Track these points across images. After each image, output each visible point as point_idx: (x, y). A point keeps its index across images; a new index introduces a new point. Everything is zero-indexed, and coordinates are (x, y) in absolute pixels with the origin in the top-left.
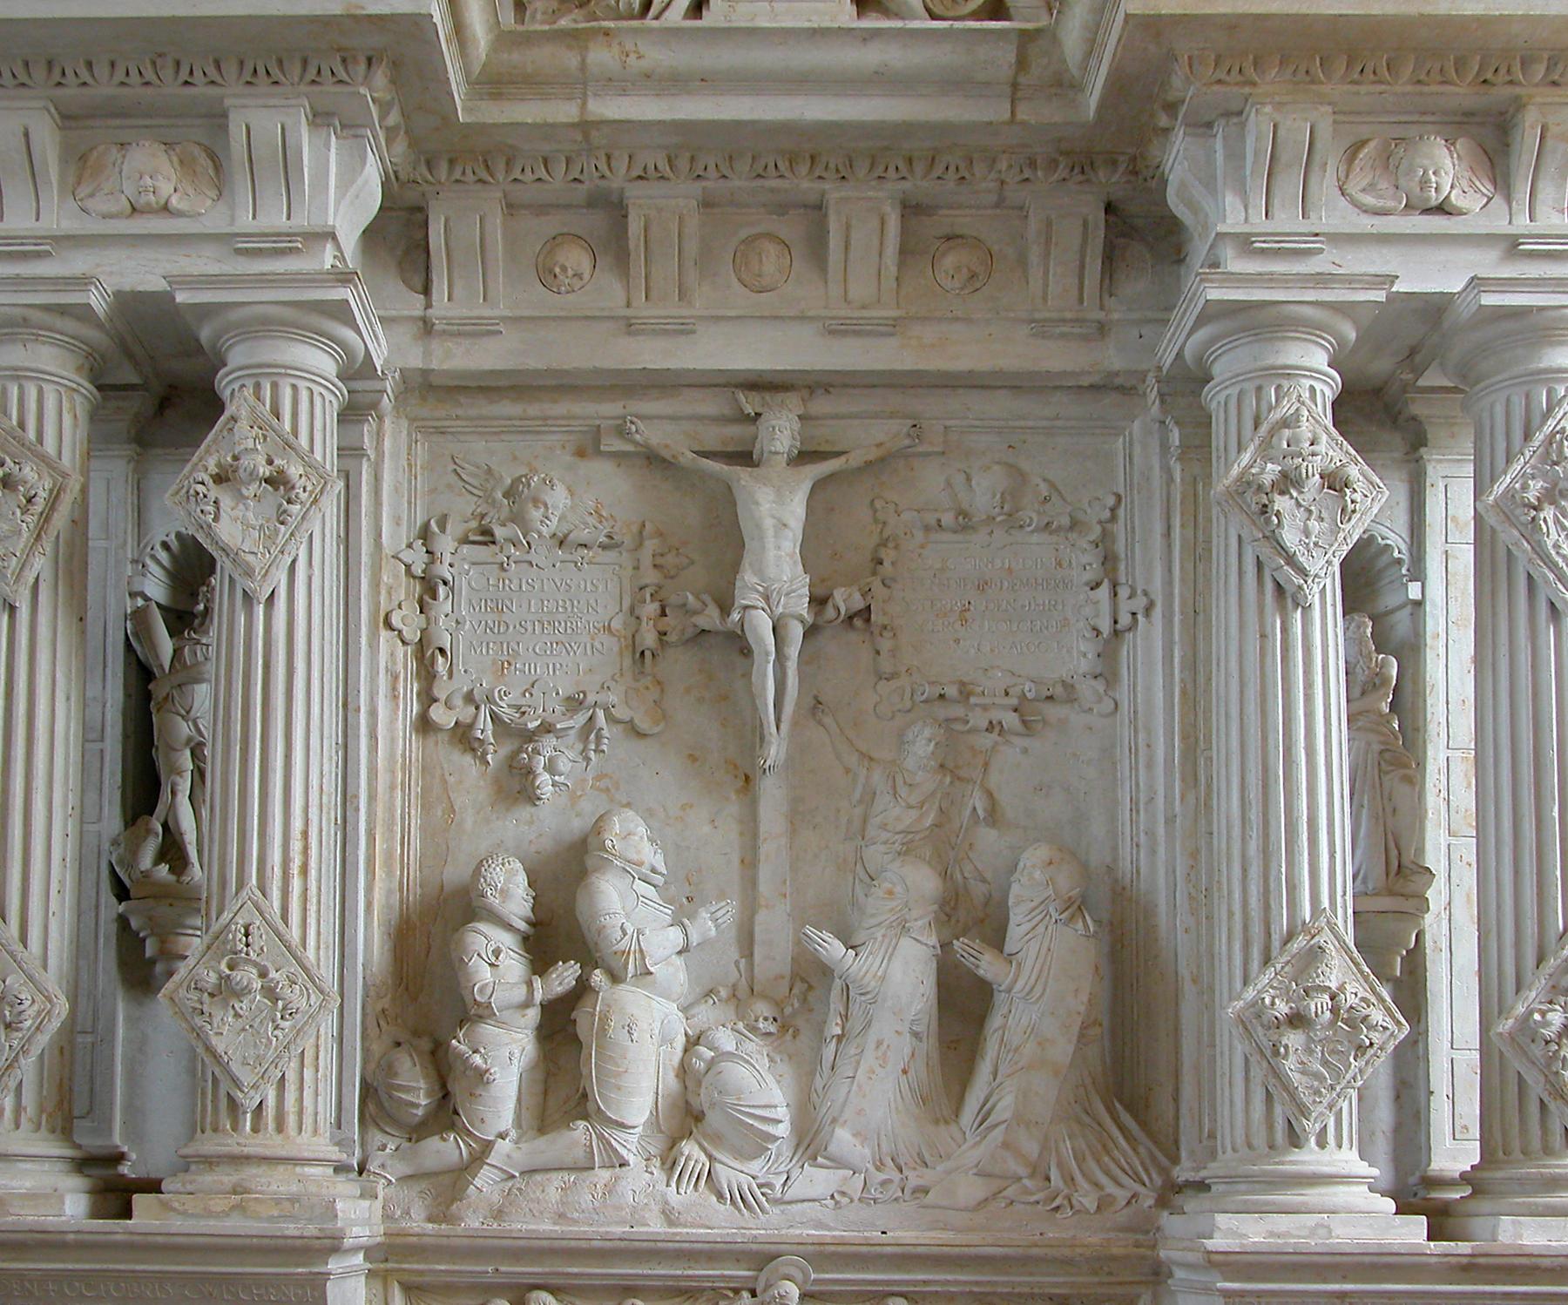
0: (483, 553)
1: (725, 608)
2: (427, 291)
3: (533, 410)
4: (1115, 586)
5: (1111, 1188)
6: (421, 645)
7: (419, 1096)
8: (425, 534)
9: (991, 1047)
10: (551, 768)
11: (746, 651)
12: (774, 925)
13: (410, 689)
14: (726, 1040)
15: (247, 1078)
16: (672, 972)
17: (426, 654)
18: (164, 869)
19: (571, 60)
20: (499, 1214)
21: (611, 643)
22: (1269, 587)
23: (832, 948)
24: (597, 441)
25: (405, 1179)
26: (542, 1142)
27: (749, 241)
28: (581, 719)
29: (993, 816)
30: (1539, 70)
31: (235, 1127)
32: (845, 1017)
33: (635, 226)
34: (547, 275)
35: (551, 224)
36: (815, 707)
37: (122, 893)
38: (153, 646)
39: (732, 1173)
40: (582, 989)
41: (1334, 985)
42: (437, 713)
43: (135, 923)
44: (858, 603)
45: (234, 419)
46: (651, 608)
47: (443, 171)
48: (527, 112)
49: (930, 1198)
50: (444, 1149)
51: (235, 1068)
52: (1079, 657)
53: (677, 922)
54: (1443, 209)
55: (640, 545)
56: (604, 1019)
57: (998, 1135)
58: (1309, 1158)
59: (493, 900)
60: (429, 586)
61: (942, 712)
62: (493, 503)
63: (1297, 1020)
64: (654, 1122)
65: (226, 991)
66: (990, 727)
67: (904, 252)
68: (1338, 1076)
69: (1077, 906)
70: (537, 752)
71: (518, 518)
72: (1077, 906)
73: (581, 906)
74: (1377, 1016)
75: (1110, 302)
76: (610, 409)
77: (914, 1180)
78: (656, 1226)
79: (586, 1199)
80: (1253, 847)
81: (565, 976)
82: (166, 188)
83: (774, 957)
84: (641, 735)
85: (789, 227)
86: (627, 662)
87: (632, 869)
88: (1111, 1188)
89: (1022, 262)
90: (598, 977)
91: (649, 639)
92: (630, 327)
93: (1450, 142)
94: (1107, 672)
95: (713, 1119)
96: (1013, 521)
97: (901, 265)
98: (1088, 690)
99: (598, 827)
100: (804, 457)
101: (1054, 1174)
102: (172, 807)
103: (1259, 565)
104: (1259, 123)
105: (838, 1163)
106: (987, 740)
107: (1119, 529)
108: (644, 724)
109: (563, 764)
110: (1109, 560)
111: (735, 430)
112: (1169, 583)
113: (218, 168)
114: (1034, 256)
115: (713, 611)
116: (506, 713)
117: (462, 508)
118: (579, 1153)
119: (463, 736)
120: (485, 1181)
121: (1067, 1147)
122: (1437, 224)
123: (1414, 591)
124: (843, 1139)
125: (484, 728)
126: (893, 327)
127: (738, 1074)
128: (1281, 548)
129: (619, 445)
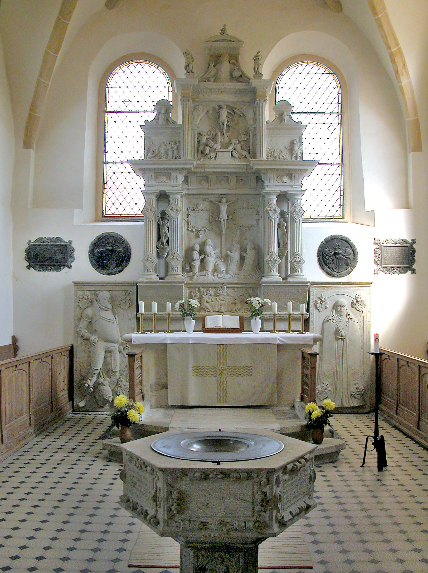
0: (194, 211)
1: (219, 218)
4: (258, 215)
7: (189, 269)
8: (187, 209)
10: (201, 234)
12: (224, 250)
15: (175, 267)
16: (213, 255)
17: (188, 223)
18: (162, 246)
19: (204, 166)
20: (197, 280)
21: (207, 221)
23: (229, 253)
26: (201, 273)
28: (204, 229)
29: (246, 239)
30: (294, 171)
34: (200, 184)
35: (201, 178)
36: (228, 228)
37: (157, 248)
38: (160, 222)
39: (220, 276)
42: (189, 228)
43: (159, 251)
44: (232, 217)
45: (172, 204)
48: (199, 170)
50: (191, 274)
51: (174, 266)
52: (254, 222)
55: (210, 210)
56: (207, 260)
58: (272, 273)
59: (196, 248)
60: (188, 215)
61: (241, 228)
62: (194, 206)
63: (270, 260)
64: (212, 271)
65: (173, 259)
67: (236, 181)
68: (274, 266)
69: (254, 248)
71: (197, 208)
72: (254, 248)
73: (204, 249)
74: (278, 260)
76: (206, 197)
78: (212, 281)
79: (205, 278)
81: (203, 256)
82: (165, 180)
83: (224, 254)
85: (225, 179)
87: (209, 245)
90: (206, 256)
91: (211, 221)
94: (257, 224)
96: (248, 208)
97: (236, 183)
98: (255, 226)
100: (227, 201)
104: (269, 175)
109: (202, 234)
110: (258, 212)
113: (170, 178)
114: (249, 182)
115: (217, 218)
116: (196, 228)
117: (191, 206)
118: (205, 274)
119: (192, 230)
120: (195, 277)
122: (286, 184)
123: (288, 216)
124: (230, 272)
125: (194, 230)
127: (220, 266)
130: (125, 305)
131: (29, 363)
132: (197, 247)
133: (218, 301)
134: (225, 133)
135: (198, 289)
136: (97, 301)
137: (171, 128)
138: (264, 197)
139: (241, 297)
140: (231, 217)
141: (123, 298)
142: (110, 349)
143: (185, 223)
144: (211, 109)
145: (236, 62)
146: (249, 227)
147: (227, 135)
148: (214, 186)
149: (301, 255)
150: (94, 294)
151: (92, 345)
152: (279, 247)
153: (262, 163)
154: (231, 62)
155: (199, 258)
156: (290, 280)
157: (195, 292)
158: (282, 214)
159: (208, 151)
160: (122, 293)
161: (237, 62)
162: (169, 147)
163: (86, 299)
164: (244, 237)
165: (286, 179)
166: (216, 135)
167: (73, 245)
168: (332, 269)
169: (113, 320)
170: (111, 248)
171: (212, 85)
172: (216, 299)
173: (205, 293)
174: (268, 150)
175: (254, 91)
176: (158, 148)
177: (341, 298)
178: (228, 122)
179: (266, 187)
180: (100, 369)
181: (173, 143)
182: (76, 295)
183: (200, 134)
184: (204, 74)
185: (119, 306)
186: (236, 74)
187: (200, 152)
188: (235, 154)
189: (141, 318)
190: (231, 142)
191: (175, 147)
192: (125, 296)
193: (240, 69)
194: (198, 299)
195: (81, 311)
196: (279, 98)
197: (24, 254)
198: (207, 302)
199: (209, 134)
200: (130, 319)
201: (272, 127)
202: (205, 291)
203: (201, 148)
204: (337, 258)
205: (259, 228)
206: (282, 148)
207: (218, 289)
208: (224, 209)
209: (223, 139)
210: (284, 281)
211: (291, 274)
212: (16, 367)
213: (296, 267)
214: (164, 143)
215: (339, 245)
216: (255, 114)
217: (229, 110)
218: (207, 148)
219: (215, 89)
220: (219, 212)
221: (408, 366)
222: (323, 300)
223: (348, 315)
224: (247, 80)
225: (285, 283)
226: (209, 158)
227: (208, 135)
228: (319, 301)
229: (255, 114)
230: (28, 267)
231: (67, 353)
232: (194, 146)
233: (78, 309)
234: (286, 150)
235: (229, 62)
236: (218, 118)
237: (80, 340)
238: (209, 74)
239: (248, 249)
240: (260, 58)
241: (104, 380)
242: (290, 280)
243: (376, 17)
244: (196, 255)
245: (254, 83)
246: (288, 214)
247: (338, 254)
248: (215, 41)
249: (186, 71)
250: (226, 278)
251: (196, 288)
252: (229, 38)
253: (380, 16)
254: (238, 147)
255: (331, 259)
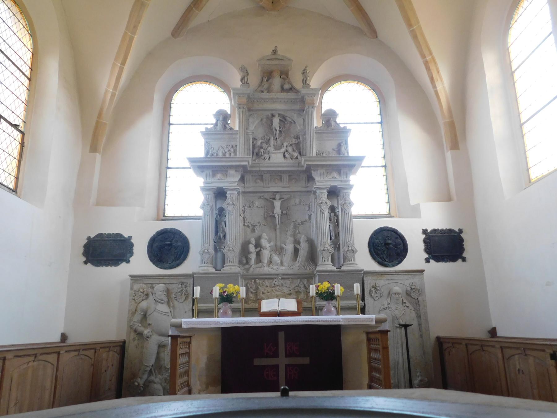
0: (250, 208)
1: (273, 213)
2: (244, 184)
3: (254, 194)
4: (310, 210)
5: (310, 268)
6: (244, 217)
7: (245, 261)
8: (244, 206)
9: (299, 255)
11: (275, 217)
13: (243, 222)
14: (274, 255)
16: (269, 249)
17: (244, 218)
18: (219, 240)
22: (321, 212)
23: (284, 246)
24: (260, 197)
25: (243, 269)
27: (275, 179)
28: (260, 224)
29: (299, 233)
31: (230, 263)
32: (285, 252)
33: (264, 178)
34: (256, 182)
36: (282, 223)
38: (218, 218)
40: (260, 250)
41: (327, 247)
42: (245, 224)
43: (216, 245)
46: (266, 213)
47: (246, 173)
48: (254, 169)
49: (294, 269)
50: (247, 266)
52: (307, 217)
53: (269, 243)
54: (335, 178)
55: (265, 207)
57: (300, 263)
59: (252, 242)
60: (244, 212)
66: (299, 224)
67: (289, 180)
69: (307, 241)
70: (255, 228)
75: (308, 184)
76: (262, 194)
77: (292, 267)
78: (268, 272)
80: (321, 235)
81: (259, 249)
84: (265, 226)
86: (264, 219)
88: (310, 268)
89: (300, 180)
90: (262, 249)
92: (264, 187)
93: (336, 172)
95: (273, 262)
97: (289, 181)
98: (308, 220)
99: (261, 235)
100: (280, 199)
101: (305, 266)
102: (220, 234)
103: (320, 210)
105: (284, 266)
106: (298, 225)
107: (310, 205)
108: (265, 225)
109: (258, 229)
111: (274, 196)
112: (315, 210)
116: (252, 224)
117: (248, 205)
120: (251, 269)
121: (306, 264)
124: (285, 264)
125: (250, 225)
126: (289, 187)
128: (322, 209)
129: (262, 198)
130: (181, 298)
131: (59, 353)
132: (253, 241)
133: (274, 293)
134: (277, 137)
135: (254, 281)
136: (152, 294)
137: (229, 134)
138: (315, 193)
139: (297, 288)
140: (285, 214)
141: (179, 290)
142: (163, 343)
143: (241, 218)
144: (265, 117)
145: (286, 78)
146: (302, 221)
147: (280, 139)
148: (268, 184)
149: (353, 244)
150: (150, 287)
151: (145, 340)
152: (331, 239)
153: (312, 159)
154: (281, 77)
155: (254, 251)
156: (343, 268)
157: (252, 284)
158: (332, 209)
159: (263, 152)
160: (179, 285)
161: (287, 77)
162: (226, 150)
163: (141, 292)
164: (298, 231)
165: (335, 174)
166: (269, 140)
167: (132, 241)
168: (383, 260)
169: (168, 313)
170: (169, 243)
171: (265, 95)
172: (272, 290)
173: (261, 285)
174: (317, 152)
175: (302, 101)
176: (216, 151)
177: (395, 286)
178: (280, 128)
179: (316, 182)
180: (151, 365)
181: (230, 147)
182: (131, 289)
183: (254, 139)
184: (258, 88)
185: (175, 299)
186: (287, 86)
187: (255, 154)
188: (287, 155)
189: (196, 311)
190: (283, 145)
191: (232, 150)
192: (182, 289)
193: (289, 83)
194: (254, 291)
195: (136, 305)
196: (324, 109)
197: (82, 250)
198: (263, 293)
199: (263, 139)
200: (186, 312)
201: (320, 132)
202: (261, 282)
203: (256, 150)
204: (388, 249)
205: (311, 223)
206: (330, 150)
207: (273, 281)
208: (277, 204)
209: (276, 142)
210: (339, 269)
211: (345, 263)
212: (35, 357)
213: (349, 256)
214: (222, 147)
215: (389, 236)
216: (304, 121)
217: (281, 118)
218: (262, 150)
219: (267, 99)
220: (273, 207)
221: (483, 350)
222: (378, 288)
223: (404, 303)
224: (297, 92)
225: (339, 271)
226: (263, 159)
227: (262, 139)
228: (373, 290)
229: (304, 121)
230: (86, 263)
231: (118, 349)
232: (250, 149)
233: (133, 302)
234: (334, 152)
235: (280, 77)
236: (271, 125)
237: (133, 335)
238: (263, 87)
239: (301, 242)
240: (308, 72)
241: (155, 378)
242: (343, 268)
243: (411, 29)
244: (252, 248)
245: (304, 91)
246: (338, 209)
247: (389, 244)
248: (268, 60)
249: (241, 83)
250: (283, 269)
251: (252, 279)
252: (279, 57)
253: (415, 27)
254: (290, 149)
255: (382, 249)
